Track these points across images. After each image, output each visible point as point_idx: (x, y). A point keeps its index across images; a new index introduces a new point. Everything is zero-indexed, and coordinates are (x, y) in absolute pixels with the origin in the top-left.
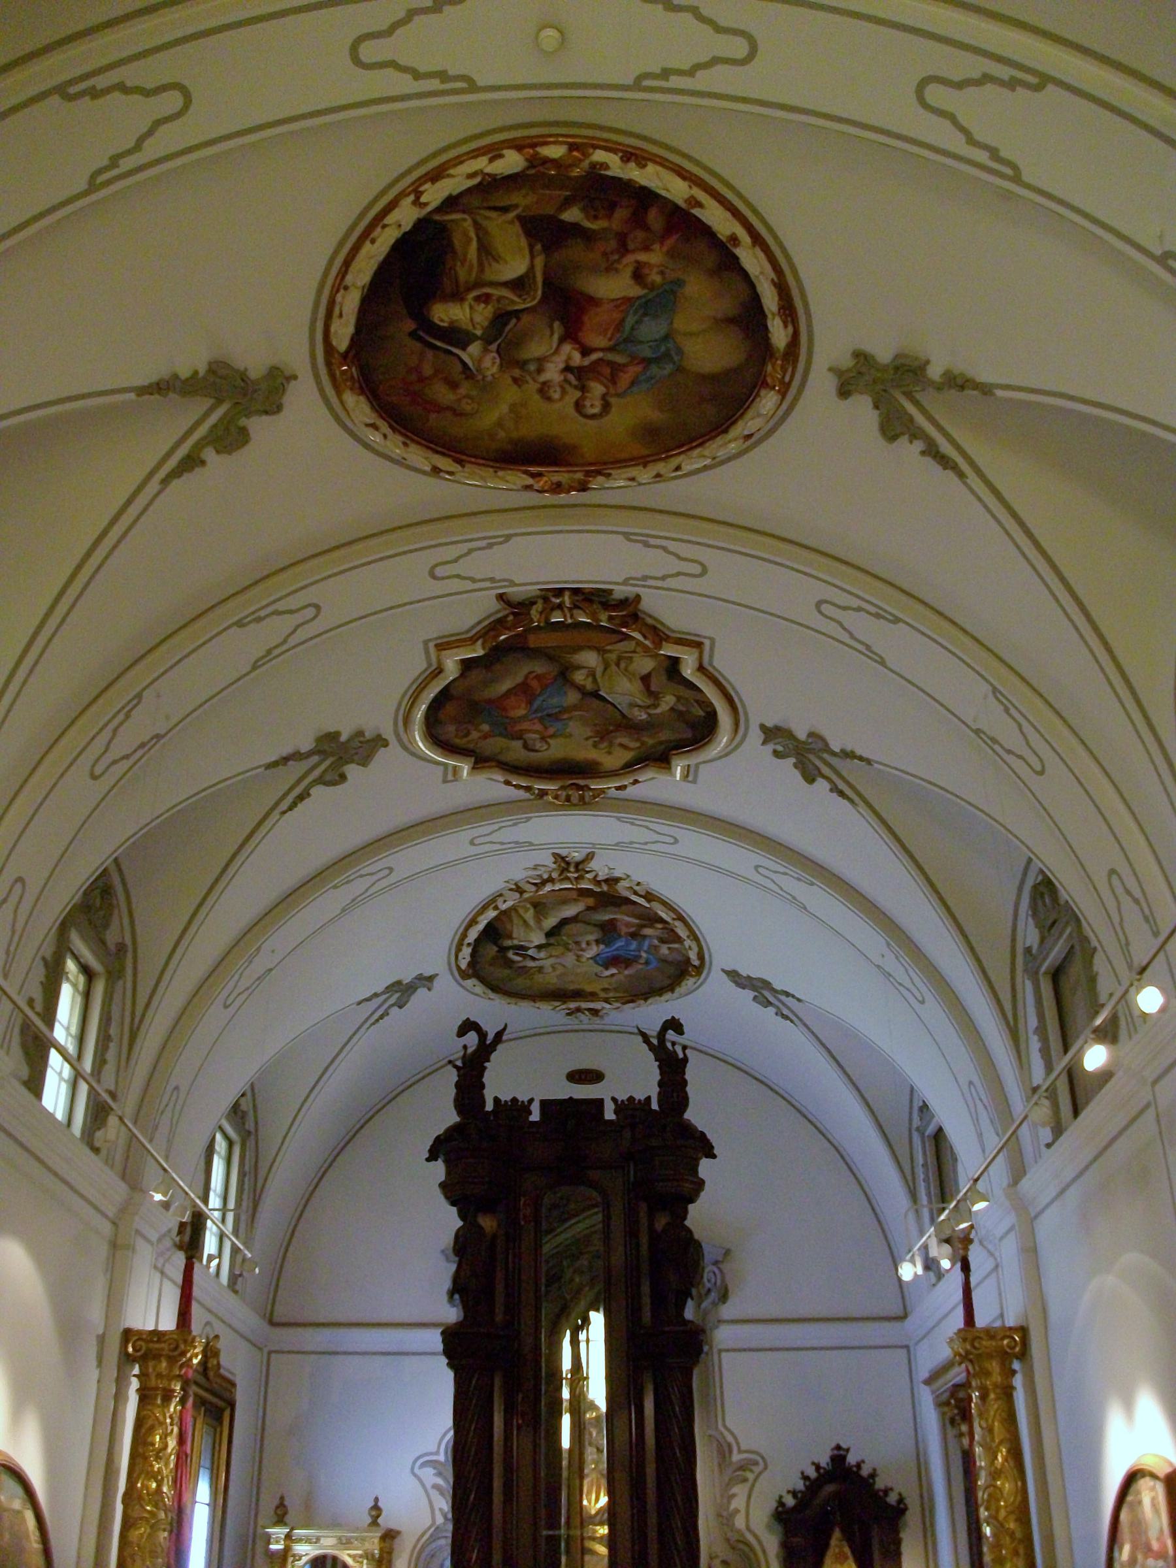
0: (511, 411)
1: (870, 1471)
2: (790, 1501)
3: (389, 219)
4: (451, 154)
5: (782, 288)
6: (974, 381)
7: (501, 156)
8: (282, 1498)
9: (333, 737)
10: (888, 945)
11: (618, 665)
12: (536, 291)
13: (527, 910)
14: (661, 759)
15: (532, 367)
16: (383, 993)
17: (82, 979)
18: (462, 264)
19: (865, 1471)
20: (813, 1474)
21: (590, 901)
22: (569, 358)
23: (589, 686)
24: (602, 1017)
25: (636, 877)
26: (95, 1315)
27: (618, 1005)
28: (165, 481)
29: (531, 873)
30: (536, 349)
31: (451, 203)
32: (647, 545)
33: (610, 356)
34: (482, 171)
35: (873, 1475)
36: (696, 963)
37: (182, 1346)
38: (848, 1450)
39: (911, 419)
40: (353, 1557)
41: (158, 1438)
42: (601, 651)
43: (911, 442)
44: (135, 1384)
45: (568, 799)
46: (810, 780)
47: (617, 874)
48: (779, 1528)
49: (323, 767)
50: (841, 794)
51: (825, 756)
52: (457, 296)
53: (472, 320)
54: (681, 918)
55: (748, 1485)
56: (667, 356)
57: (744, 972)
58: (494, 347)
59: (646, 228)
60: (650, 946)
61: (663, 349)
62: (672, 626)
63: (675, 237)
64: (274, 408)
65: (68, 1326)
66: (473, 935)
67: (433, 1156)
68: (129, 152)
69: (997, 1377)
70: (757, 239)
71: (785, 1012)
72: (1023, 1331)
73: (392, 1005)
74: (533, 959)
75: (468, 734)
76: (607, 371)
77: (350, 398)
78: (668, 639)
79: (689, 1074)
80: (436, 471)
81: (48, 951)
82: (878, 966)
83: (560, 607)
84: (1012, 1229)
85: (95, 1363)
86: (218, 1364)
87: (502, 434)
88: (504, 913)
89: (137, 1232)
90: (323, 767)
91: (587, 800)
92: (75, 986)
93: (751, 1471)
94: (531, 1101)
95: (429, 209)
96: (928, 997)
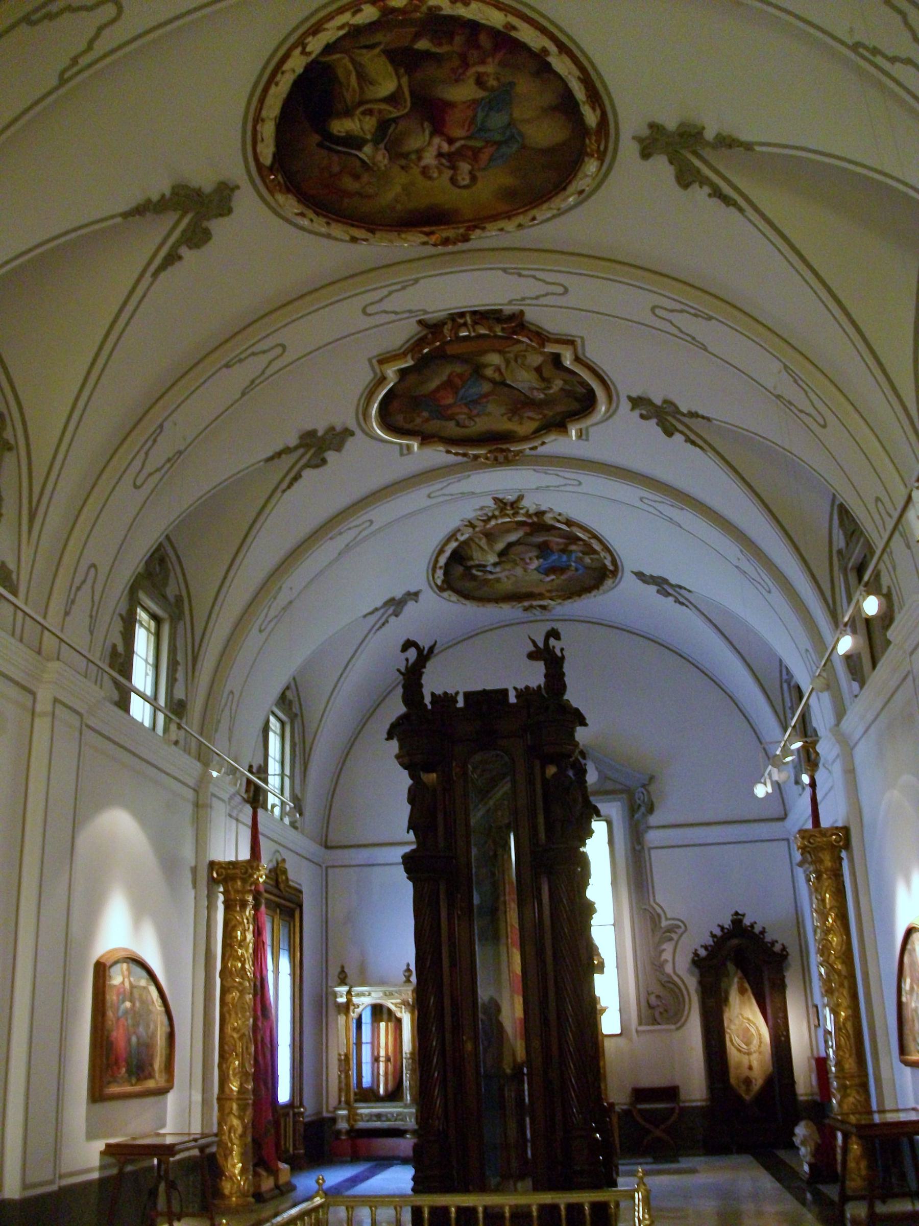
0: (403, 189)
1: (761, 929)
2: (703, 953)
3: (286, 67)
4: (322, 14)
5: (587, 81)
6: (738, 141)
7: (360, 10)
8: (343, 967)
9: (312, 434)
10: (741, 551)
11: (516, 361)
12: (405, 102)
13: (480, 539)
14: (559, 425)
15: (413, 157)
16: (381, 608)
17: (153, 624)
18: (348, 90)
19: (757, 930)
20: (718, 932)
21: (527, 529)
22: (440, 147)
23: (497, 376)
24: (550, 611)
25: (557, 509)
26: (188, 853)
27: (560, 601)
28: (155, 275)
29: (479, 513)
30: (414, 143)
31: (329, 49)
32: (520, 275)
33: (471, 143)
34: (347, 23)
35: (763, 932)
36: (611, 568)
37: (250, 871)
38: (744, 915)
39: (698, 171)
40: (395, 1005)
41: (239, 933)
42: (500, 352)
43: (701, 187)
44: (221, 898)
45: (496, 459)
46: (669, 433)
47: (543, 508)
48: (696, 971)
49: (308, 456)
50: (693, 443)
51: (679, 416)
52: (348, 113)
53: (362, 129)
54: (595, 537)
55: (673, 943)
56: (512, 137)
57: (647, 572)
58: (382, 146)
59: (478, 47)
60: (576, 557)
61: (508, 133)
62: (552, 331)
63: (502, 53)
64: (225, 210)
65: (169, 864)
66: (442, 561)
67: (390, 736)
68: (84, 52)
69: (828, 864)
70: (563, 48)
71: (682, 600)
72: (846, 830)
73: (390, 615)
74: (491, 573)
75: (412, 421)
76: (470, 153)
77: (280, 198)
78: (549, 340)
79: (566, 668)
80: (354, 240)
81: (123, 608)
82: (737, 567)
83: (465, 324)
84: (838, 756)
85: (190, 886)
86: (287, 879)
87: (399, 207)
88: (465, 543)
89: (213, 795)
90: (308, 456)
91: (510, 458)
92: (148, 630)
93: (676, 932)
94: (457, 693)
95: (313, 56)
96: (774, 590)
